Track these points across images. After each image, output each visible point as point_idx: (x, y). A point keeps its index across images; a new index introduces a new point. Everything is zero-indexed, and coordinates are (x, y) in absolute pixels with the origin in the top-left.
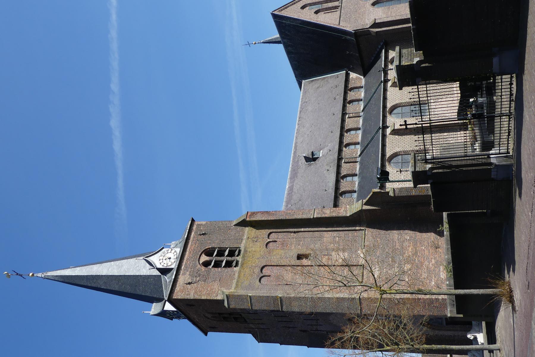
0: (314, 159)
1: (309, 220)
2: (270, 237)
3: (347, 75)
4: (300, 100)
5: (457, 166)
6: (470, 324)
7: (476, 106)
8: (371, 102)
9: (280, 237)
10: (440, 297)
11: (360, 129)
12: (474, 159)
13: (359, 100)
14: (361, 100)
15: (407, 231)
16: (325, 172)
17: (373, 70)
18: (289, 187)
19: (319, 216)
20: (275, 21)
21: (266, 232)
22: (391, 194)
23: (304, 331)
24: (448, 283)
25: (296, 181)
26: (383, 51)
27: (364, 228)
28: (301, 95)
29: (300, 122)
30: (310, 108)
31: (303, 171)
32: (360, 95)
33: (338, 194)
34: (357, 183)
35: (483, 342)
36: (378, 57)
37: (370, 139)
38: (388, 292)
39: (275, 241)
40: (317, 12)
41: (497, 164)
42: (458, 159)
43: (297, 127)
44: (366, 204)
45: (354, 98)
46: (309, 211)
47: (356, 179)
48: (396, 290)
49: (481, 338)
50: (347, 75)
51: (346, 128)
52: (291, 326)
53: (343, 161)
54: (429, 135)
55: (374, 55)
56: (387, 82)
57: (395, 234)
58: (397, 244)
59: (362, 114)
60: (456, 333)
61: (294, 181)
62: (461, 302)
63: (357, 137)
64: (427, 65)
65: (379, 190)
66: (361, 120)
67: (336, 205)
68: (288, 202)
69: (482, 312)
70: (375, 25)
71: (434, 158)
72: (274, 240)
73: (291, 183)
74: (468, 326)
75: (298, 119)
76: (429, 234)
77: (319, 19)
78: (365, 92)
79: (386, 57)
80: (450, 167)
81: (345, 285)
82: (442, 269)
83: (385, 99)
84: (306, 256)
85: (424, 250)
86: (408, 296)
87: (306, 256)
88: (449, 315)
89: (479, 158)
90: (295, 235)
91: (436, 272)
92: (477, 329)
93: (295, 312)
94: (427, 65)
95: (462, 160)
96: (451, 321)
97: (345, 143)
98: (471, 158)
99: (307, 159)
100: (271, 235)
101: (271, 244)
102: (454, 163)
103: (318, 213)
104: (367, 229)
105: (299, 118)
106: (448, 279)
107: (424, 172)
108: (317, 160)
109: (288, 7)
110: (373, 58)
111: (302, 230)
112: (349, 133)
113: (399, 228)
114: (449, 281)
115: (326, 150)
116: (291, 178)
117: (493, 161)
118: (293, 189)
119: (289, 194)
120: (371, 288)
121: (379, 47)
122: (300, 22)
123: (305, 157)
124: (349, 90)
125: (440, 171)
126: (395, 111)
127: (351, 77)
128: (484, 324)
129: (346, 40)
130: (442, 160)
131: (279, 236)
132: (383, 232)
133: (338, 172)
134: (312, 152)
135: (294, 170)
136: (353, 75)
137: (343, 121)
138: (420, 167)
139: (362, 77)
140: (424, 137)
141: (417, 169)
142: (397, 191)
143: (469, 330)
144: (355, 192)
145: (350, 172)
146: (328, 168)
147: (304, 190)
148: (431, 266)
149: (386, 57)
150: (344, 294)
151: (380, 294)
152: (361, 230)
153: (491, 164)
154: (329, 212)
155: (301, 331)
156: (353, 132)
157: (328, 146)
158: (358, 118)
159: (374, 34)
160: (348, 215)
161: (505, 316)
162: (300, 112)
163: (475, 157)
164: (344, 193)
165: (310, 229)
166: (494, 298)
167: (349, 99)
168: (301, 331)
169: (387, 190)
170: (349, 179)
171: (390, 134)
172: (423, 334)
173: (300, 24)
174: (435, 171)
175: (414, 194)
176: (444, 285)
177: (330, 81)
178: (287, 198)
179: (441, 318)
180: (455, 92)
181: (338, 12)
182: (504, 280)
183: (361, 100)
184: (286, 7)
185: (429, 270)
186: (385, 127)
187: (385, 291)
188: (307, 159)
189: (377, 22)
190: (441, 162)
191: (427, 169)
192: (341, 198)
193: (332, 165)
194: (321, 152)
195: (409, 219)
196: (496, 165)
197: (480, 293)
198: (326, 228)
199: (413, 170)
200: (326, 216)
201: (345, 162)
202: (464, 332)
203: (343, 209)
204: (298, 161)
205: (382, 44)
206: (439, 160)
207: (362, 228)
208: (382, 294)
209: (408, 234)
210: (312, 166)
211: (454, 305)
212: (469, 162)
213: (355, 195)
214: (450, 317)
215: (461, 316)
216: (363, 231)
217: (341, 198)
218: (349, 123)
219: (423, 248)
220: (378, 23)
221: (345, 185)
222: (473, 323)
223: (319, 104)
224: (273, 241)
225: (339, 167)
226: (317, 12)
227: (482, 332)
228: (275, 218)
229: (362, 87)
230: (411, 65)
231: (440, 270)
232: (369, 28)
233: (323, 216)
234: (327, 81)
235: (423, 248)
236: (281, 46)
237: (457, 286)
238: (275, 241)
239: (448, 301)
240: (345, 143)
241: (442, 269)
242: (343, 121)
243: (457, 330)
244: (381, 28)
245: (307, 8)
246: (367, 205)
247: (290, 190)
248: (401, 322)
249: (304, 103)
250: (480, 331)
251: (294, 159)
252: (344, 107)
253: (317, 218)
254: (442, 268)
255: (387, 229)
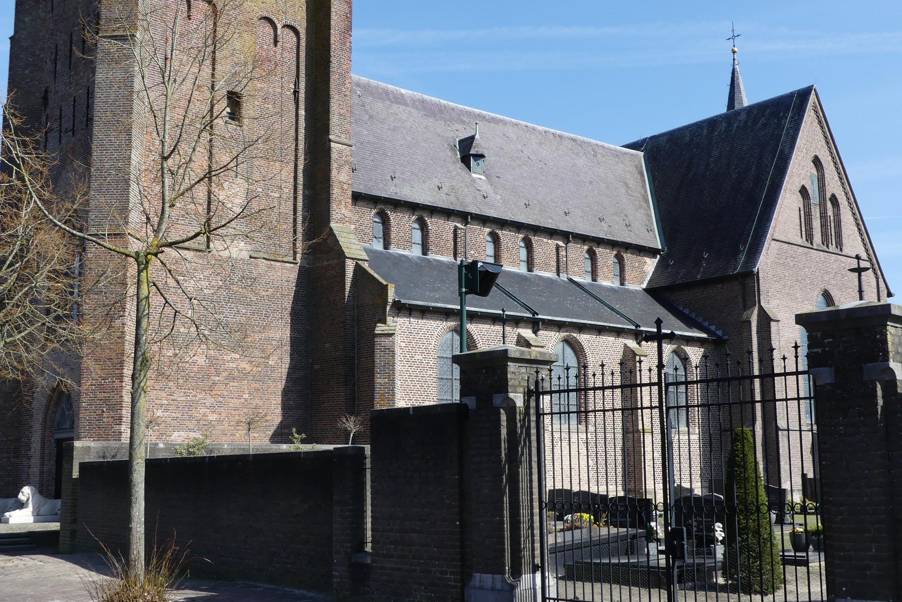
0: (466, 160)
1: (327, 131)
2: (287, 30)
3: (651, 252)
4: (600, 143)
5: (514, 480)
6: (57, 496)
7: (634, 537)
8: (591, 299)
9: (286, 54)
10: (125, 428)
11: (530, 270)
12: (532, 527)
13: (594, 274)
14: (594, 280)
15: (287, 360)
16: (436, 182)
17: (661, 311)
18: (402, 95)
19: (334, 155)
20: (791, 95)
21: (300, 20)
22: (380, 328)
23: (45, 98)
24: (161, 446)
25: (415, 113)
26: (704, 335)
27: (299, 260)
28: (612, 146)
29: (551, 137)
30: (581, 162)
31: (439, 130)
32: (607, 278)
33: (384, 206)
34: (406, 253)
35: (10, 522)
36: (690, 323)
37: (510, 290)
38: (144, 274)
39: (276, 42)
40: (804, 191)
41: (518, 591)
42: (535, 484)
43: (540, 128)
44: (358, 269)
45: (600, 262)
46: (347, 132)
47: (415, 252)
48: (147, 298)
49: (21, 519)
50: (651, 252)
51: (534, 239)
52: (59, 66)
53: (459, 225)
54: (618, 404)
55: (693, 315)
56: (636, 339)
57: (281, 332)
58: (257, 337)
59: (564, 277)
60: (35, 461)
61: (417, 108)
62: (114, 474)
63: (513, 263)
64: (880, 402)
65: (390, 300)
66: (550, 275)
67: (357, 197)
68: (366, 88)
69: (86, 526)
70: (766, 320)
71: (539, 415)
72: (280, 39)
73: (414, 101)
74: (52, 488)
75: (558, 132)
76: (279, 411)
77: (788, 195)
78: (612, 290)
79: (689, 341)
80: (514, 460)
81: (165, 159)
82: (192, 435)
83: (600, 330)
84: (235, 115)
85: (240, 397)
86: (130, 338)
87: (235, 115)
88: (77, 444)
89: (533, 542)
90: (290, 93)
91: (187, 423)
92: (43, 510)
93: (94, 73)
94: (880, 402)
95: (531, 494)
96: (64, 451)
97: (499, 232)
98: (536, 519)
99: (466, 144)
100: (292, 34)
101: (269, 30)
102: (523, 471)
103: (340, 152)
104: (297, 267)
105: (560, 136)
106: (170, 447)
107: (503, 386)
108: (463, 165)
109: (822, 127)
110: (687, 311)
111: (302, 112)
112: (522, 244)
113: (295, 343)
114: (167, 449)
115: (486, 188)
116: (423, 101)
117: (526, 579)
118: (400, 103)
119: (386, 92)
120: (156, 231)
121: (713, 328)
122: (787, 151)
123: (472, 138)
124: (619, 252)
125: (504, 431)
126: (569, 351)
127: (648, 260)
128: (55, 526)
129: (737, 252)
130: (534, 438)
131: (288, 54)
132: (288, 304)
133: (434, 211)
134: (482, 156)
135: (441, 112)
136: (650, 265)
137: (552, 233)
138: (518, 377)
139: (644, 286)
140: (613, 387)
141: (512, 367)
142: (386, 341)
143: (42, 491)
144: (386, 246)
145: (432, 238)
146: (445, 189)
147: (395, 129)
148: (203, 411)
149: (689, 341)
150: (141, 157)
151: (137, 253)
152: (295, 253)
153: (517, 573)
154: (342, 180)
155: (46, 91)
156: (523, 253)
157: (496, 193)
158: (554, 269)
159: (745, 316)
160: (333, 225)
161: (69, 584)
162: (574, 140)
163: (537, 532)
164: (385, 221)
165: (302, 131)
166: (119, 561)
167: (599, 251)
168: (46, 91)
169: (389, 319)
170: (417, 236)
171: (519, 335)
172: (23, 372)
173: (782, 151)
174: (504, 417)
175: (379, 381)
176: (154, 438)
177: (640, 214)
178: (377, 88)
179: (72, 427)
180: (610, 487)
181: (799, 241)
182: (171, 586)
183: (594, 280)
184: (823, 121)
185: (190, 406)
186: (536, 325)
187: (146, 268)
188: (466, 144)
189: (772, 324)
190: (528, 435)
191: (511, 395)
192: (374, 211)
193: (452, 198)
194: (483, 177)
195: (317, 367)
196: (513, 588)
197: (133, 525)
198: (305, 171)
199: (511, 355)
200: (334, 173)
201: (456, 229)
202: (37, 479)
203: (349, 214)
204: (463, 122)
205: (720, 333)
206: (533, 431)
207: (299, 256)
208: (137, 256)
209: (280, 363)
210: (450, 153)
211: (104, 457)
212: (524, 512)
213: (378, 246)
214: (71, 449)
215: (76, 474)
216: (291, 259)
217: (374, 211)
218: (545, 247)
219: (246, 396)
220: (770, 327)
221: (402, 222)
222: (59, 502)
223: (591, 183)
224: (276, 36)
225: (447, 213)
226: (804, 191)
227: (35, 522)
228: (333, 47)
229: (622, 284)
230: (886, 353)
231: (190, 430)
232: (761, 308)
233: (334, 165)
234: (641, 207)
235: (246, 396)
236: (722, 109)
237: (152, 466)
238: (276, 42)
239: (113, 444)
240: (499, 232)
241: (192, 435)
242: (552, 233)
243: (42, 464)
244: (758, 333)
245: (814, 171)
246: (355, 271)
247: (395, 97)
248: (58, 319)
249: (595, 151)
250: (39, 516)
251: (469, 114)
252: (583, 239)
253: (329, 148)
254: (198, 435)
255: (294, 314)
